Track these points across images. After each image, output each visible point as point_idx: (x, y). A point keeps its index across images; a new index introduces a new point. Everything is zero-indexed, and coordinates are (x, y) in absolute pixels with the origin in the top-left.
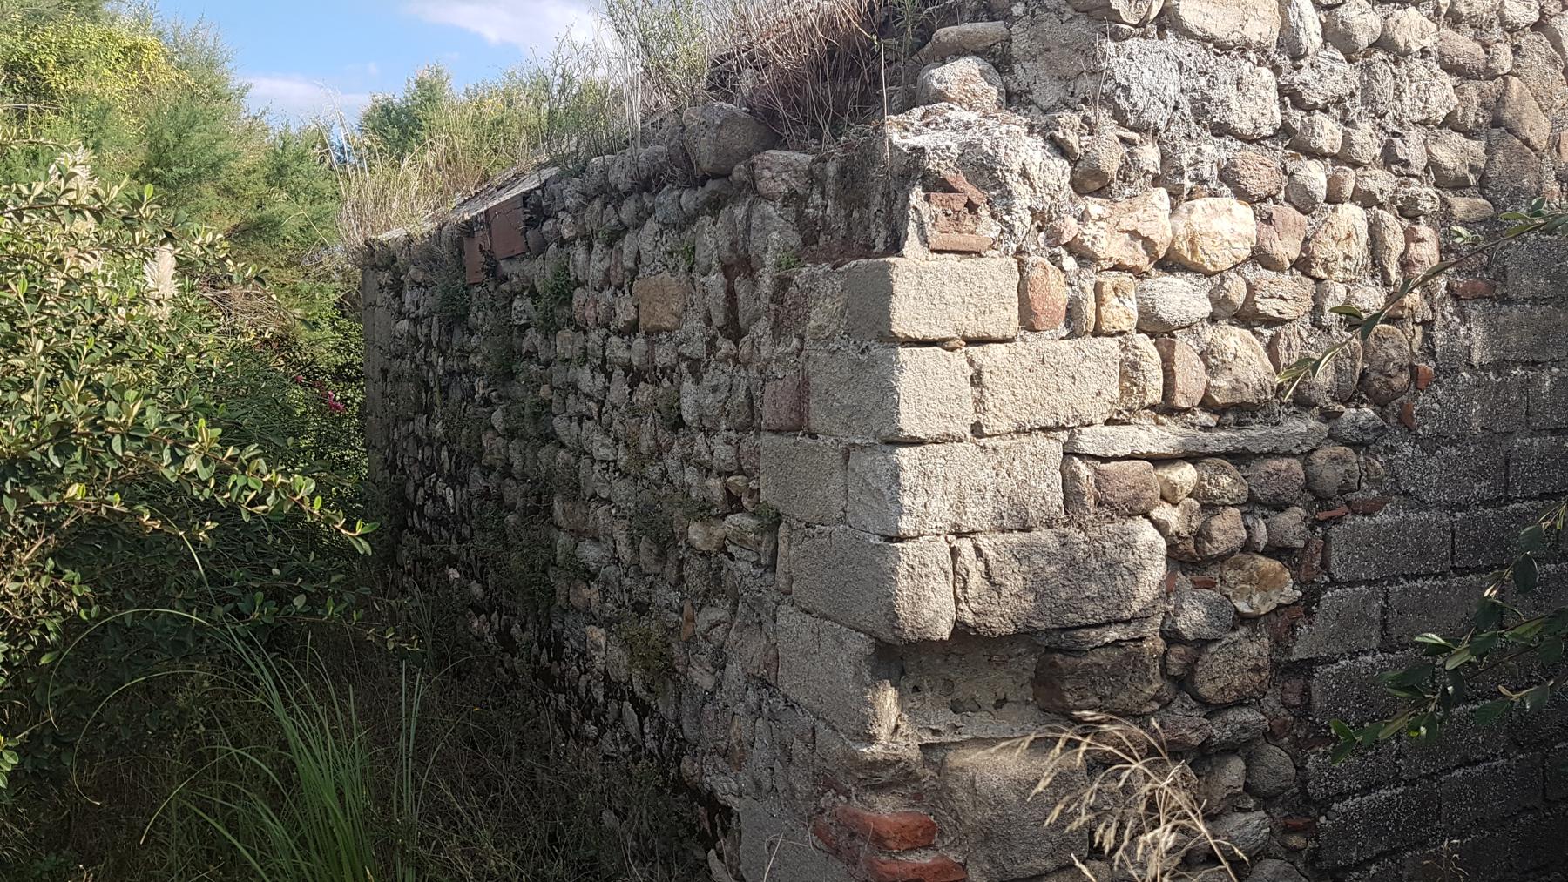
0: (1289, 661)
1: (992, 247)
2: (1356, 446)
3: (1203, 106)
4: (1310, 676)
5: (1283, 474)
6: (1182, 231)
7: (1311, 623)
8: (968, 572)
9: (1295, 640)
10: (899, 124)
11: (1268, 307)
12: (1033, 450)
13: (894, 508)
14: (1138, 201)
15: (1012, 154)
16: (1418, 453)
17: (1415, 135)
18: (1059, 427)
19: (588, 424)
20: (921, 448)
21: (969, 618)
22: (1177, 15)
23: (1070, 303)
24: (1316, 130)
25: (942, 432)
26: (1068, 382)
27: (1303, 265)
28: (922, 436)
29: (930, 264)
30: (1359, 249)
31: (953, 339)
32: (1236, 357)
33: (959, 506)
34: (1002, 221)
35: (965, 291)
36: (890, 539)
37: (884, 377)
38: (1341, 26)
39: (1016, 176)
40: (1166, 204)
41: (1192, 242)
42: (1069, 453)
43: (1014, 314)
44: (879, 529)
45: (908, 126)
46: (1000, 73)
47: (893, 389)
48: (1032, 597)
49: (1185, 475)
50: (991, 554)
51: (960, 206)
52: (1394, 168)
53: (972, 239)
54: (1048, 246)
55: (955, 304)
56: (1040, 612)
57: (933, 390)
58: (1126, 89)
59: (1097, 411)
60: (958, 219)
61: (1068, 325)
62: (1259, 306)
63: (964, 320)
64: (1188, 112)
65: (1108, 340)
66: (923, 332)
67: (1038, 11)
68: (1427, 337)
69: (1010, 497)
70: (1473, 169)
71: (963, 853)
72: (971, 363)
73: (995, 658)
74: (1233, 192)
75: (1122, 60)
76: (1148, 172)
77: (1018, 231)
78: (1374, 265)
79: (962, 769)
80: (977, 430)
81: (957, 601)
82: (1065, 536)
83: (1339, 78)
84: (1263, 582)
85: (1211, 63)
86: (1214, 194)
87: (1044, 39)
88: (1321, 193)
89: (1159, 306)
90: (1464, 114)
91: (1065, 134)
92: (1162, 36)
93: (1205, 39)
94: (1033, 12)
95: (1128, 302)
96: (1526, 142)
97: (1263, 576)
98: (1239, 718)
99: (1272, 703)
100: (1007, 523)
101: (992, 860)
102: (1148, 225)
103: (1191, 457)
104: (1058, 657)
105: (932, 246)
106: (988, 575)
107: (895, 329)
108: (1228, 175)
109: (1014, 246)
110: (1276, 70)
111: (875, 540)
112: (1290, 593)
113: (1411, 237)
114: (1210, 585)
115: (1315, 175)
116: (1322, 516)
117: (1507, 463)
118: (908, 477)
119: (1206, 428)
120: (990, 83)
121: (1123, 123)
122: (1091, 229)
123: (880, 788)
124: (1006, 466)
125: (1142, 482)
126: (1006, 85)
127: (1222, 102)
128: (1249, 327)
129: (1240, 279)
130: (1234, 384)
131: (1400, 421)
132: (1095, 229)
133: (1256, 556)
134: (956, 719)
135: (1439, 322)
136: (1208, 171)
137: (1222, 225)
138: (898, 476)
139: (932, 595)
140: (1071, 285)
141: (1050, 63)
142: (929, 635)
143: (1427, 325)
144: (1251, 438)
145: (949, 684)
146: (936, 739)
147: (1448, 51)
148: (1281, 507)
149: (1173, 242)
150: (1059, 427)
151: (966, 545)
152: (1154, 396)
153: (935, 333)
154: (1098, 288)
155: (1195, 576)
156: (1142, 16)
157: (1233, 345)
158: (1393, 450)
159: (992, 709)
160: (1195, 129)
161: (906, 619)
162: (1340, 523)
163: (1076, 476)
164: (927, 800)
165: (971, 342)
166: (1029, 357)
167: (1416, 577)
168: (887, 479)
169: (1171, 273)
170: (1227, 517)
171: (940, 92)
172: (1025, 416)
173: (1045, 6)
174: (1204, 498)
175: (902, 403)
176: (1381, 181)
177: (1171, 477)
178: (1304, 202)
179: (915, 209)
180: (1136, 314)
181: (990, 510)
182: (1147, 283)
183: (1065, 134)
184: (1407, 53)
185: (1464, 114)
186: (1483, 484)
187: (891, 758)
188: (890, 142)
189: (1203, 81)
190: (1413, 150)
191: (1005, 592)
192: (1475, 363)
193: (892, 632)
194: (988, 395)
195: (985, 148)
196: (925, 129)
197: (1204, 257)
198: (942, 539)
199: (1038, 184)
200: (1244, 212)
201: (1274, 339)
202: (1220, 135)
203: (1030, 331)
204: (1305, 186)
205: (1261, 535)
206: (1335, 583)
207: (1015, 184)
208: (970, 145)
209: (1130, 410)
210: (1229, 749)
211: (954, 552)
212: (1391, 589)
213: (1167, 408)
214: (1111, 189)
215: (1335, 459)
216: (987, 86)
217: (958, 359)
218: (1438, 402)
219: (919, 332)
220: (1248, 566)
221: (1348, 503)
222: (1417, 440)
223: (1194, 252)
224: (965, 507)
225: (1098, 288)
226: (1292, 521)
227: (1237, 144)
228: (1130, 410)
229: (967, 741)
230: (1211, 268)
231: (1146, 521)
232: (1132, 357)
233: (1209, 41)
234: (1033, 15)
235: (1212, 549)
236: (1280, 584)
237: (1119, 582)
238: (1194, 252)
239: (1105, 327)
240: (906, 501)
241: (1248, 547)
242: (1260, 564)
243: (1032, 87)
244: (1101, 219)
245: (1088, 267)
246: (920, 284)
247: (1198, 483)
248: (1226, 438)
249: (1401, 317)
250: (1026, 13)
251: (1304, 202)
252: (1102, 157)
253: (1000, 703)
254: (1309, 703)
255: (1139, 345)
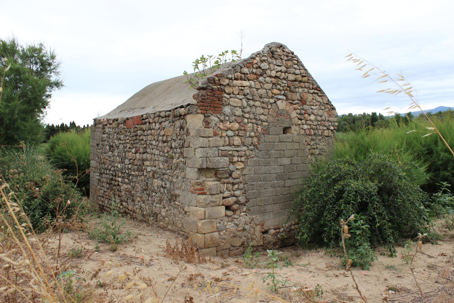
2: (251, 151)
19: (154, 150)
30: (251, 129)
40: (229, 123)
59: (221, 145)
84: (240, 165)
112: (243, 167)
114: (234, 165)
145: (206, 175)
148: (242, 157)
151: (208, 159)
153: (205, 136)
176: (254, 121)
205: (239, 160)
210: (236, 184)
226: (243, 159)
241: (238, 161)
253: (211, 177)
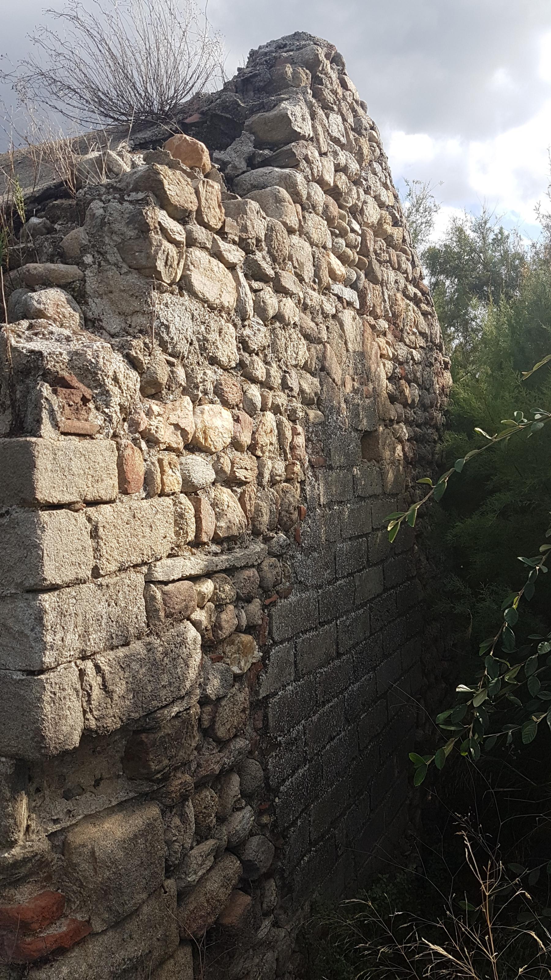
0: (258, 700)
1: (99, 432)
3: (204, 344)
4: (267, 707)
5: (252, 579)
6: (200, 426)
7: (266, 672)
8: (91, 687)
9: (260, 685)
10: (12, 331)
11: (241, 474)
12: (129, 582)
13: (38, 646)
14: (177, 404)
15: (108, 363)
16: (303, 558)
17: (293, 372)
18: (144, 563)
20: (57, 593)
21: (93, 724)
22: (190, 281)
23: (146, 473)
24: (255, 366)
25: (72, 577)
26: (148, 530)
27: (252, 448)
28: (59, 582)
29: (62, 443)
31: (77, 502)
32: (228, 506)
33: (85, 636)
34: (103, 412)
35: (85, 465)
36: (32, 673)
37: (27, 536)
38: (262, 304)
39: (110, 380)
41: (204, 432)
42: (149, 581)
43: (115, 481)
44: (22, 665)
45: (20, 333)
46: (79, 303)
47: (37, 546)
48: (131, 696)
49: (208, 587)
50: (106, 668)
51: (78, 400)
52: (286, 391)
53: (87, 425)
54: (130, 432)
55: (79, 475)
56: (135, 705)
57: (66, 544)
58: (167, 327)
59: (163, 549)
60: (77, 409)
61: (145, 490)
62: (237, 474)
63: (85, 487)
64: (197, 347)
65: (167, 498)
66: (58, 497)
67: (103, 263)
68: (303, 490)
69: (117, 622)
70: (316, 394)
71: (87, 911)
72: (89, 520)
73: (99, 749)
74: (221, 401)
75: (162, 307)
76: (181, 385)
77: (114, 421)
78: (280, 448)
79: (84, 846)
80: (96, 572)
81: (85, 712)
82: (150, 643)
83: (263, 335)
84: (244, 651)
85: (207, 317)
86: (212, 402)
87: (108, 284)
88: (259, 405)
89: (192, 474)
90: (311, 363)
91: (136, 353)
92: (182, 295)
93: (204, 301)
94: (100, 263)
95: (177, 473)
96: (334, 380)
97: (245, 646)
98: (238, 747)
99: (250, 730)
100: (115, 642)
101: (109, 909)
102: (184, 420)
103: (208, 575)
104: (143, 736)
105: (62, 429)
106: (104, 686)
107: (39, 496)
108: (218, 391)
109: (112, 431)
110: (235, 325)
111: (17, 676)
113: (295, 433)
115: (254, 391)
116: (267, 602)
117: (335, 559)
118: (50, 618)
119: (216, 554)
120: (74, 310)
121: (165, 350)
122: (154, 422)
123: (17, 883)
124: (115, 597)
125: (189, 596)
126: (84, 313)
127: (214, 343)
128: (230, 487)
129: (226, 457)
130: (228, 524)
131: (295, 540)
132: (156, 421)
133: (240, 634)
134: (70, 805)
135: (307, 481)
136: (210, 387)
137: (218, 422)
138: (42, 619)
139: (68, 713)
140: (145, 460)
141: (112, 302)
142: (67, 747)
143: (302, 483)
144: (237, 558)
145: (62, 778)
146: (57, 827)
147: (304, 325)
148: (249, 600)
149: (195, 433)
150: (144, 563)
152: (191, 537)
153: (66, 498)
154: (160, 461)
155: (211, 655)
156: (172, 277)
157: (226, 499)
158: (293, 557)
159: (93, 789)
160: (202, 359)
161: (51, 739)
162: (275, 605)
163: (154, 598)
164: (55, 878)
165: (90, 504)
166: (126, 514)
167: (306, 631)
168: (32, 621)
169: (193, 453)
170: (228, 611)
171: (40, 311)
172: (124, 559)
173: (108, 260)
174: (217, 601)
175: (46, 558)
177: (202, 590)
178: (251, 410)
179: (46, 399)
180: (181, 480)
181: (104, 634)
182: (183, 459)
183: (136, 353)
184: (289, 324)
185: (311, 363)
186: (328, 572)
187: (29, 855)
188: (11, 345)
189: (203, 328)
190: (293, 382)
191: (115, 697)
192: (322, 504)
193: (39, 751)
194: (102, 544)
195: (89, 357)
196: (35, 338)
197: (211, 443)
198: (73, 664)
199: (124, 387)
200: (227, 414)
201: (243, 494)
202: (212, 365)
203: (124, 494)
204: (252, 400)
206: (275, 643)
207: (111, 386)
208: (76, 353)
209: (178, 546)
211: (82, 673)
212: (297, 641)
213: (197, 544)
214: (162, 394)
215: (271, 566)
216: (72, 311)
217: (81, 517)
218: (309, 527)
219: (56, 497)
220: (237, 642)
221: (277, 592)
222: (303, 550)
223: (206, 439)
224: (88, 635)
225: (160, 461)
227: (220, 371)
228: (178, 546)
229: (80, 820)
230: (214, 450)
231: (189, 622)
232: (179, 510)
233: (205, 302)
234: (100, 265)
235: (224, 634)
236: (252, 649)
237: (179, 670)
238: (206, 439)
239: (167, 490)
240: (49, 638)
242: (243, 639)
243: (102, 317)
244: (159, 415)
245: (153, 448)
246: (54, 459)
247: (214, 592)
248: (226, 559)
249: (293, 479)
250: (94, 263)
251: (251, 410)
252: (159, 372)
253: (97, 783)
254: (267, 725)
255: (182, 502)
